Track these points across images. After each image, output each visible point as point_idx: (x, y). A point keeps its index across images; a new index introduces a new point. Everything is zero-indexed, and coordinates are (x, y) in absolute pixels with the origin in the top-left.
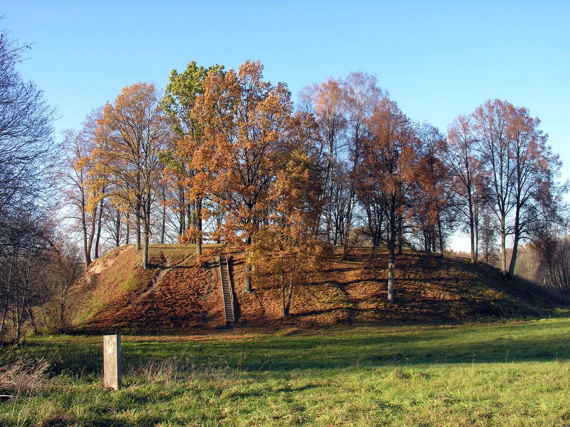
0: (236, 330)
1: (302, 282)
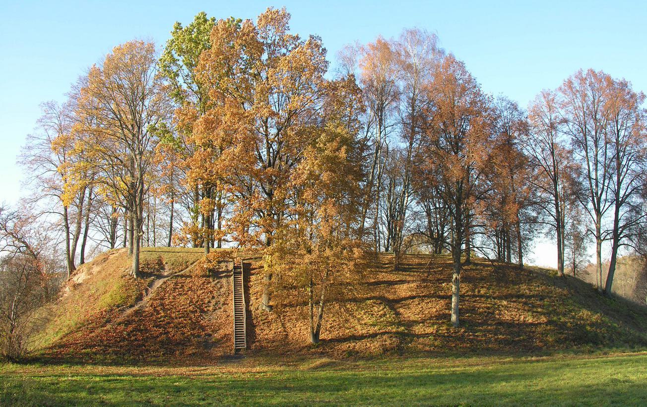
0: (246, 361)
1: (338, 296)
